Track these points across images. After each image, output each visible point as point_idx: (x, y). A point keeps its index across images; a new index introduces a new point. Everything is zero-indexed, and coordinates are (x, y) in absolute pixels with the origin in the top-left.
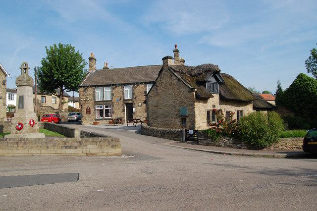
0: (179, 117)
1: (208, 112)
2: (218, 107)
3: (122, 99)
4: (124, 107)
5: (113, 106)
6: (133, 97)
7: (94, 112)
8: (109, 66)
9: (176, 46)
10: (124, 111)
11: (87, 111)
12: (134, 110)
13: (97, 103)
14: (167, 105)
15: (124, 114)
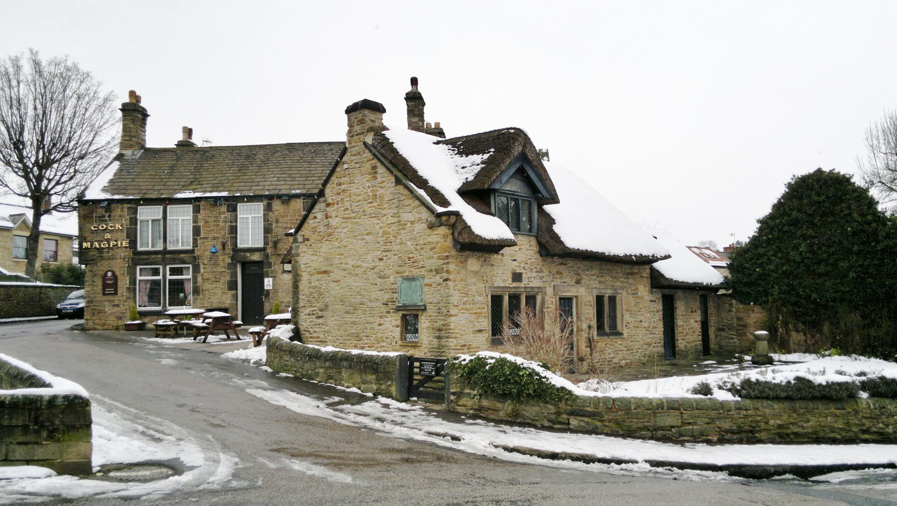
0: (398, 309)
1: (496, 301)
2: (531, 281)
3: (229, 246)
4: (234, 275)
5: (196, 270)
6: (266, 243)
7: (132, 289)
8: (198, 140)
9: (414, 81)
10: (232, 286)
11: (105, 286)
12: (268, 283)
13: (139, 258)
14: (359, 271)
15: (235, 297)
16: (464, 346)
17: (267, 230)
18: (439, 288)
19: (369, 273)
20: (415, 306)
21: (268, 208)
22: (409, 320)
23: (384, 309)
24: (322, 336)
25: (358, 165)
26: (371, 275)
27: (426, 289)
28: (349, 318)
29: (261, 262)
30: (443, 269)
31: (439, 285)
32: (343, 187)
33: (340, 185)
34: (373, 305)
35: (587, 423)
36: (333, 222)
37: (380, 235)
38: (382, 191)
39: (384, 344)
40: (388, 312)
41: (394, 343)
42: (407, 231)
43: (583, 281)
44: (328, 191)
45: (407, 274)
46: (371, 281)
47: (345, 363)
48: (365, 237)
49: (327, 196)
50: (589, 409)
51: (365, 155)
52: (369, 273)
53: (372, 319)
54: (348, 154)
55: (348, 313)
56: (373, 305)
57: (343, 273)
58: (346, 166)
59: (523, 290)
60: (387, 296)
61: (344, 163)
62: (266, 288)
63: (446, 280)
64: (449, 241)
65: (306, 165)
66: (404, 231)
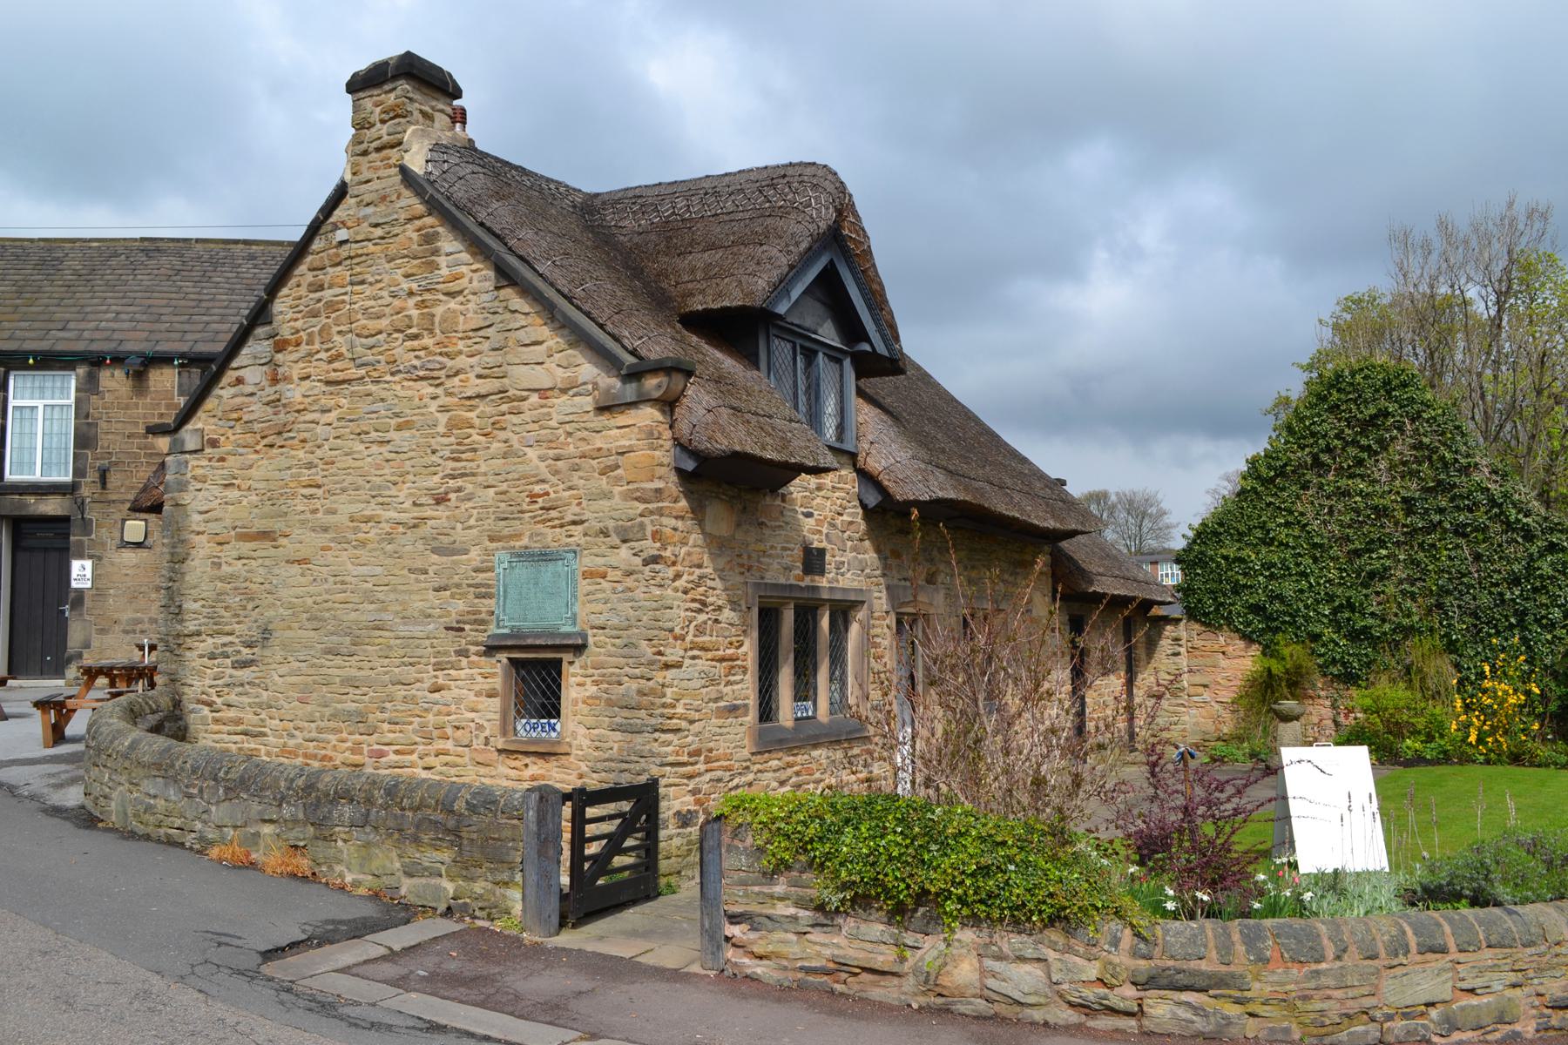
0: (491, 650)
6: (79, 472)
12: (81, 572)
16: (697, 753)
17: (84, 440)
18: (629, 582)
19: (402, 540)
20: (552, 635)
21: (89, 387)
22: (537, 677)
23: (449, 643)
24: (249, 716)
25: (379, 232)
26: (409, 543)
27: (584, 586)
28: (337, 669)
29: (65, 520)
30: (642, 526)
31: (629, 574)
32: (327, 294)
33: (321, 288)
34: (417, 630)
35: (1195, 1009)
36: (294, 393)
37: (441, 429)
38: (453, 304)
39: (449, 745)
40: (463, 653)
41: (478, 744)
42: (527, 416)
43: (940, 578)
44: (280, 306)
45: (525, 541)
46: (408, 563)
47: (347, 811)
48: (392, 435)
49: (278, 319)
50: (1203, 966)
51: (403, 203)
52: (402, 540)
53: (411, 674)
54: (349, 201)
55: (333, 652)
56: (417, 630)
57: (323, 539)
58: (342, 234)
59: (825, 596)
60: (460, 605)
61: (336, 227)
62: (74, 584)
63: (655, 560)
64: (665, 454)
65: (188, 287)
66: (515, 419)
